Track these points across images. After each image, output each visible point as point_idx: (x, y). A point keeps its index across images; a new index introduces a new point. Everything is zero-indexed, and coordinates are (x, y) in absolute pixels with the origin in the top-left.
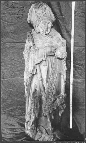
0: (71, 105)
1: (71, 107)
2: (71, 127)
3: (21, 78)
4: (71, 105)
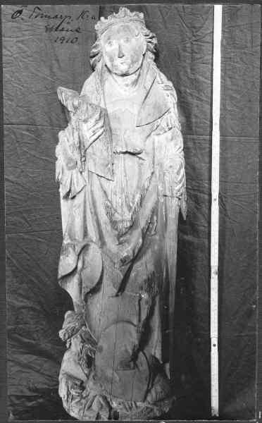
0: (214, 340)
1: (215, 200)
2: (218, 9)
3: (26, 237)
4: (214, 340)
